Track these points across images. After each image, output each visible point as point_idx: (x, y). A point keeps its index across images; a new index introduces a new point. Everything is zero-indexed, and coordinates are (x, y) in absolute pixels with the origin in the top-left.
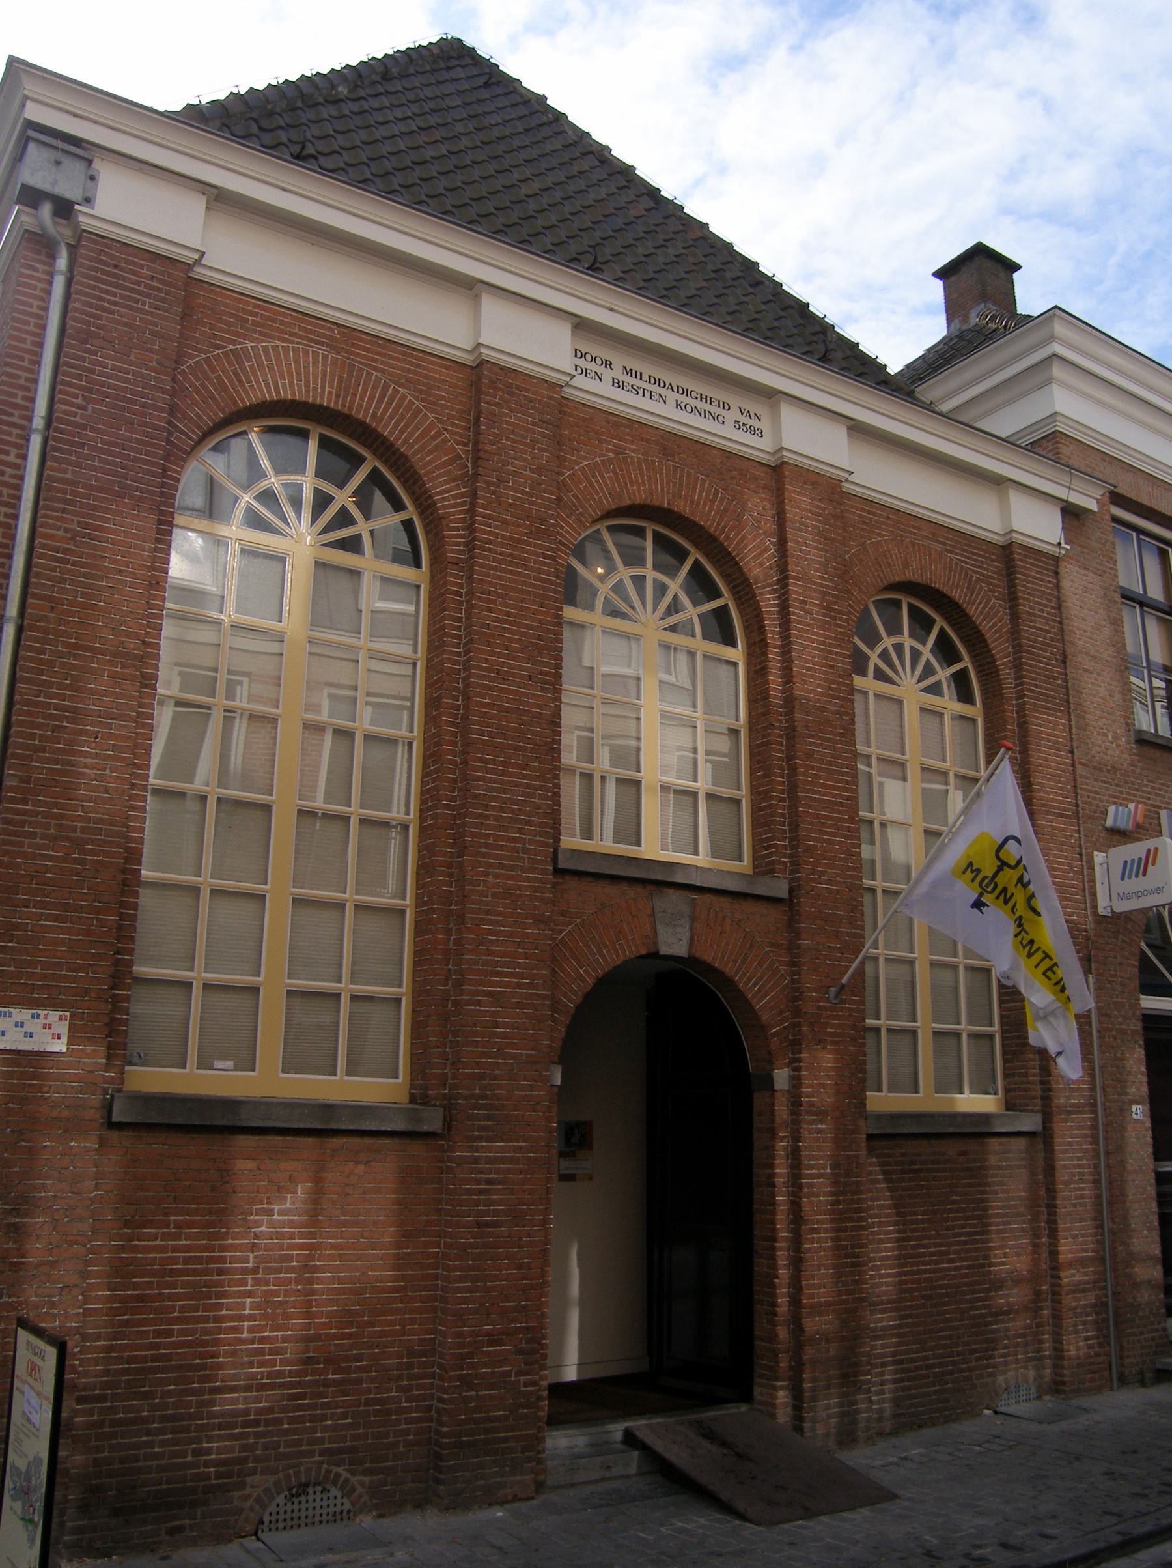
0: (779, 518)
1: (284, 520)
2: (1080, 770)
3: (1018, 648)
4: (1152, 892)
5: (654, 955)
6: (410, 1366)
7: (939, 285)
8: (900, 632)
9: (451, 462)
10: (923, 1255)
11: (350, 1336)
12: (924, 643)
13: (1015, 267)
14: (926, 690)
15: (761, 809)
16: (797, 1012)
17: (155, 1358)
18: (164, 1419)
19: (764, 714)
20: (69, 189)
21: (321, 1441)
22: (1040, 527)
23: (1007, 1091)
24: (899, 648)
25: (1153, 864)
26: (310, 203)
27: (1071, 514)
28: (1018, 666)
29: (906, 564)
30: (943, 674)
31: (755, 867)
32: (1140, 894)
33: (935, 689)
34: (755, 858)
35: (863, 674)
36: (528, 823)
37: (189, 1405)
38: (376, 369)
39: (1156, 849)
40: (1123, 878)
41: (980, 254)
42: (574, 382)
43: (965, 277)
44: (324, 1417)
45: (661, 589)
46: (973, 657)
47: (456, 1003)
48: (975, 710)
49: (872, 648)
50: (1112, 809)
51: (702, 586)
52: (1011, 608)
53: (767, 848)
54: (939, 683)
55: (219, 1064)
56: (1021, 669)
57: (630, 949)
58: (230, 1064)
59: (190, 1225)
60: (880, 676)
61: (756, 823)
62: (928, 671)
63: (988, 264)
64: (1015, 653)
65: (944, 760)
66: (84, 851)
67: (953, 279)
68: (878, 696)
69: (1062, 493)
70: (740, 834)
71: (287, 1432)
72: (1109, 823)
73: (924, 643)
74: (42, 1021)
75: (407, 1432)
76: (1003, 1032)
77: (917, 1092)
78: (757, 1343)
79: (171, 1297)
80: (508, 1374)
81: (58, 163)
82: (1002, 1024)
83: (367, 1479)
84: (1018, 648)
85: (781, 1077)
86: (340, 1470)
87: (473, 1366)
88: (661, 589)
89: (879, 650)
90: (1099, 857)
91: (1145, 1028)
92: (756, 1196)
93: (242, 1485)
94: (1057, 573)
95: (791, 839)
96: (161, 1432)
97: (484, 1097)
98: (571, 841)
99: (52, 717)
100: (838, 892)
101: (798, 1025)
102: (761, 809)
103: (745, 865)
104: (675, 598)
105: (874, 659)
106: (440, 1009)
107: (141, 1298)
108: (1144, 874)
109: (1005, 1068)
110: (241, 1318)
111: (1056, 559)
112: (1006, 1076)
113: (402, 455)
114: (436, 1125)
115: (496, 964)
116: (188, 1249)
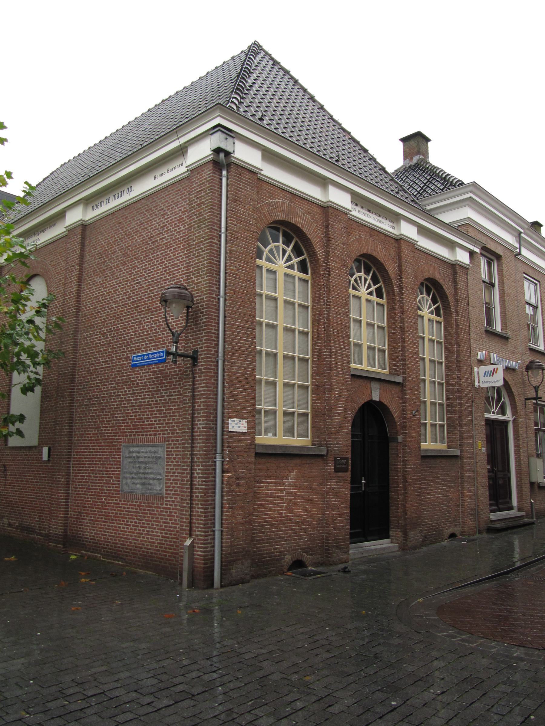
0: (399, 257)
1: (275, 258)
2: (472, 341)
3: (456, 300)
4: (495, 382)
5: (371, 400)
6: (319, 524)
7: (401, 144)
8: (368, 275)
9: (320, 241)
10: (431, 493)
11: (306, 515)
12: (288, 247)
13: (428, 140)
14: (288, 267)
15: (392, 354)
16: (405, 418)
17: (265, 522)
18: (268, 539)
19: (394, 323)
20: (229, 149)
21: (301, 545)
22: (463, 257)
23: (448, 443)
24: (277, 248)
25: (496, 373)
26: (283, 149)
27: (472, 254)
28: (456, 306)
29: (429, 272)
30: (295, 261)
31: (390, 372)
32: (490, 382)
33: (291, 267)
34: (390, 370)
35: (261, 258)
36: (345, 360)
37: (272, 535)
38: (301, 209)
39: (497, 368)
40: (484, 376)
41: (419, 135)
42: (351, 213)
43: (412, 143)
44: (301, 539)
45: (284, 252)
46: (442, 302)
47: (329, 416)
48: (384, 301)
49: (265, 248)
50: (479, 353)
51: (297, 251)
52: (454, 286)
53: (395, 366)
54: (293, 265)
55: (269, 434)
56: (457, 307)
57: (366, 399)
58: (271, 434)
59: (271, 483)
60: (269, 260)
61: (390, 358)
62: (289, 259)
63: (420, 139)
64: (455, 301)
65: (433, 336)
66: (247, 371)
67: (408, 143)
68: (377, 304)
69: (472, 247)
70: (294, 344)
71: (293, 543)
72: (479, 357)
73: (288, 247)
74: (241, 423)
75: (319, 543)
76: (447, 424)
77: (426, 442)
78: (391, 518)
79: (268, 504)
80: (343, 526)
81: (226, 139)
82: (447, 421)
83: (310, 557)
84: (456, 300)
85: (400, 438)
86: (304, 554)
87: (336, 523)
88: (284, 252)
89: (269, 248)
90: (476, 369)
91: (486, 424)
92: (390, 474)
93: (283, 558)
94: (467, 274)
95: (403, 364)
96: (267, 543)
97: (337, 444)
98: (476, 384)
99: (237, 329)
100: (415, 381)
101: (405, 422)
102: (392, 354)
103: (387, 371)
104: (289, 255)
105: (266, 251)
106: (321, 417)
107: (261, 504)
108: (492, 376)
109: (447, 435)
110: (282, 510)
111: (467, 269)
112: (448, 438)
113: (309, 238)
114: (324, 453)
115: (339, 404)
116: (271, 490)
